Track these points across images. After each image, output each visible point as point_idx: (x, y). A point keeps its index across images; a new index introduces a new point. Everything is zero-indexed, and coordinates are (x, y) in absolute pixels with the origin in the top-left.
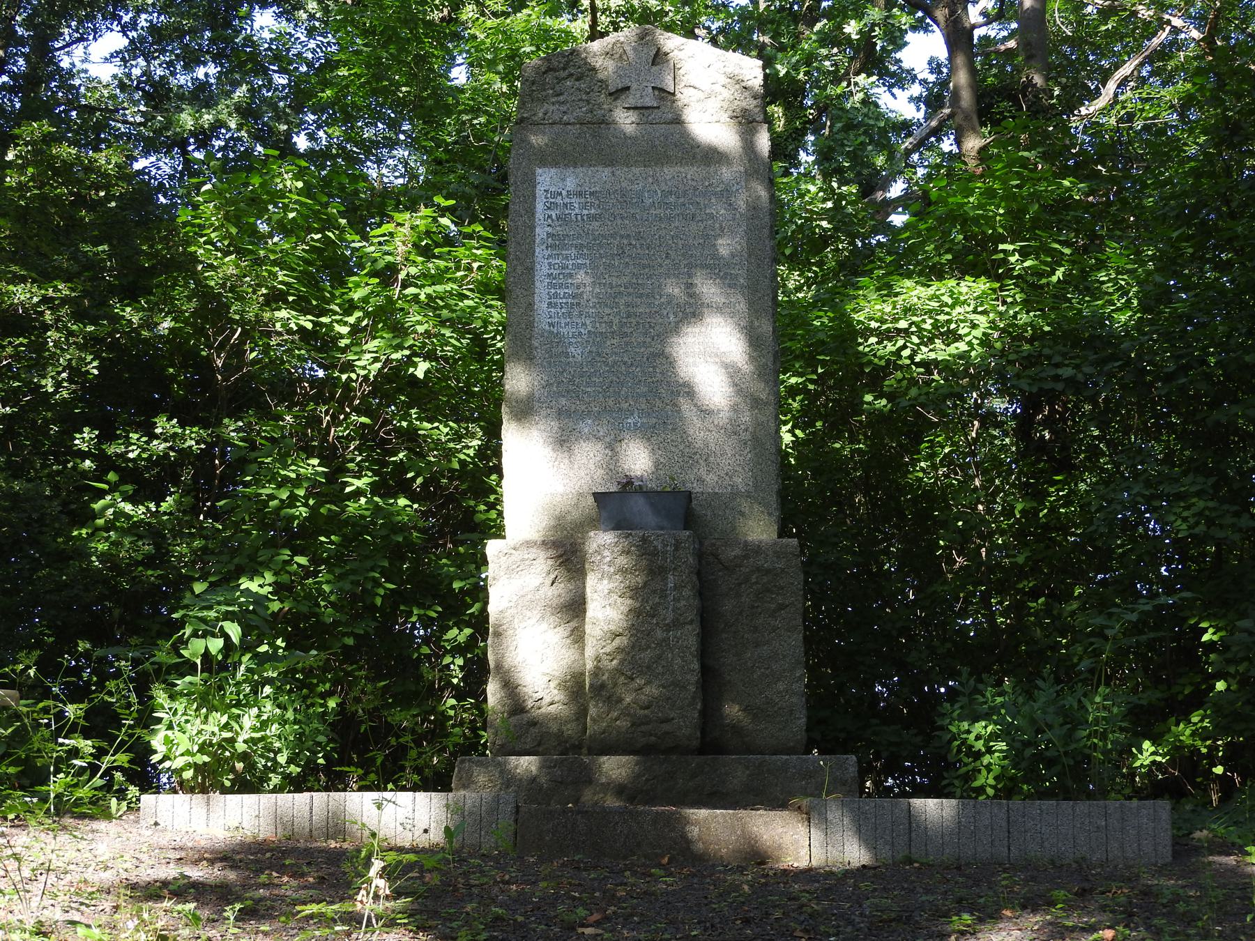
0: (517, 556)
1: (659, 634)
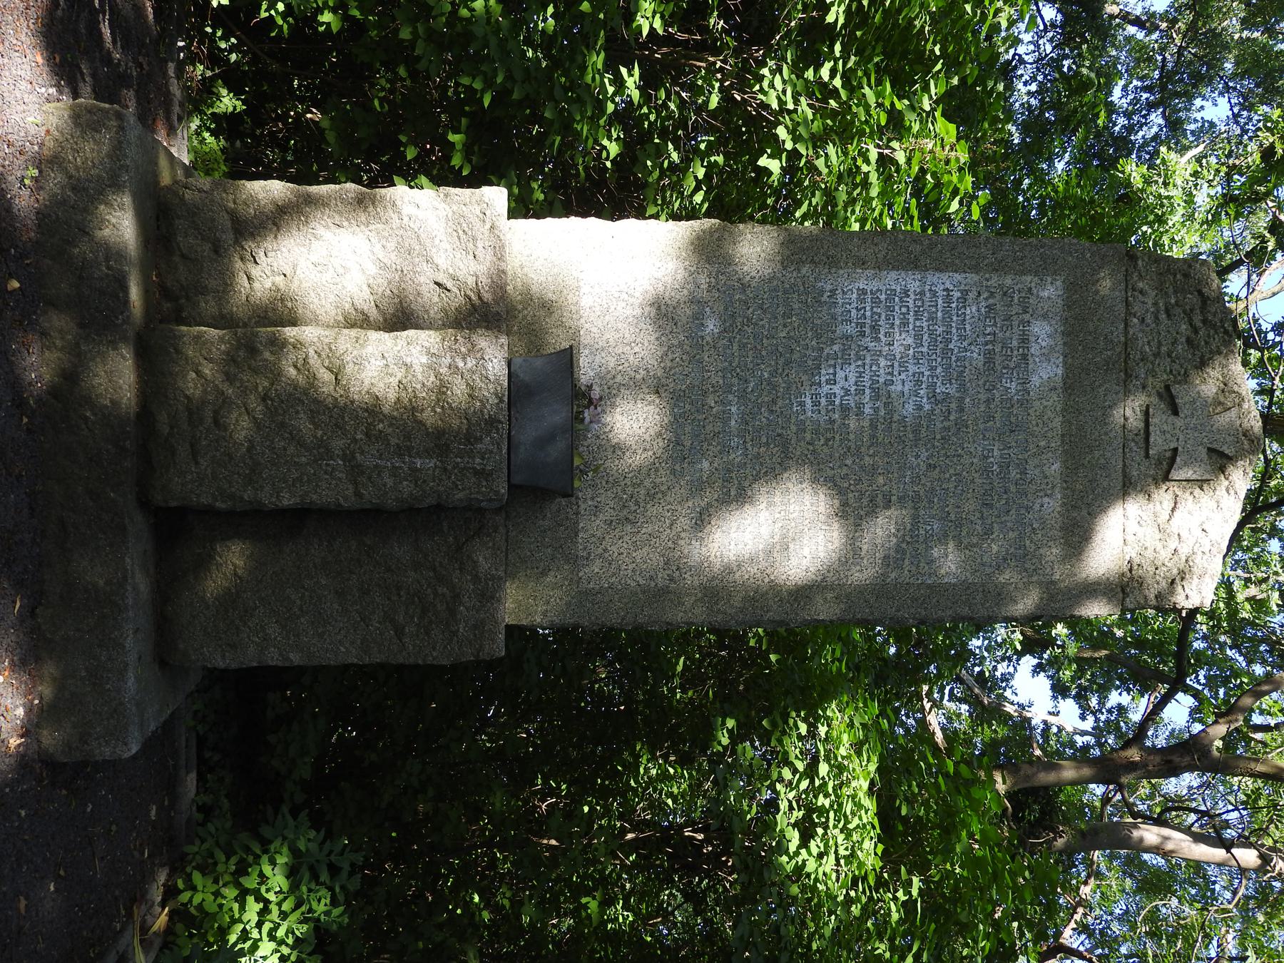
0: (482, 230)
1: (338, 444)
